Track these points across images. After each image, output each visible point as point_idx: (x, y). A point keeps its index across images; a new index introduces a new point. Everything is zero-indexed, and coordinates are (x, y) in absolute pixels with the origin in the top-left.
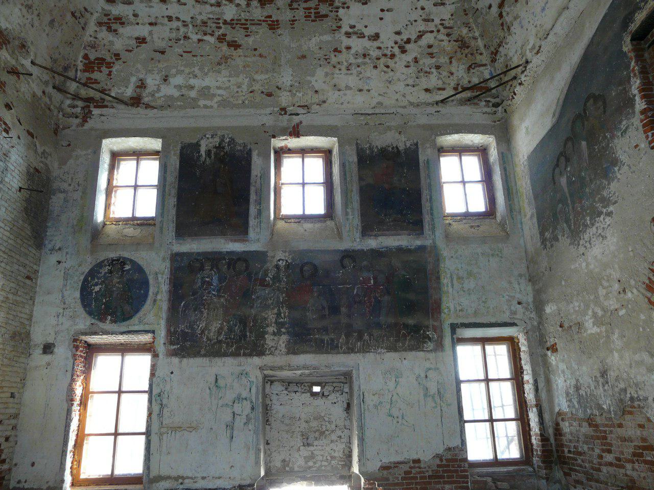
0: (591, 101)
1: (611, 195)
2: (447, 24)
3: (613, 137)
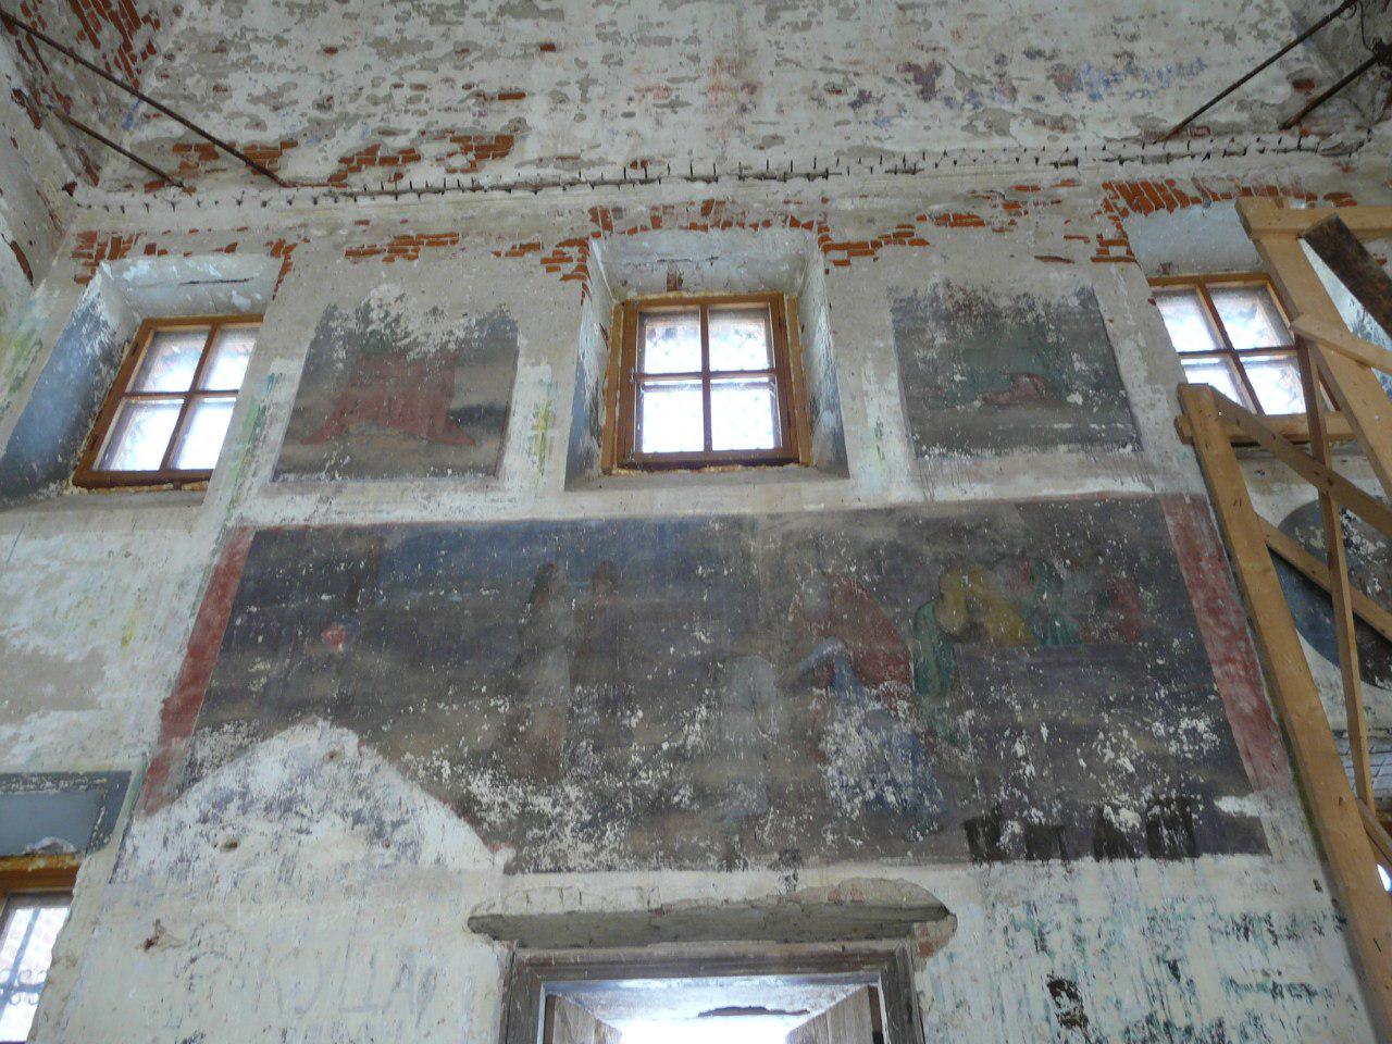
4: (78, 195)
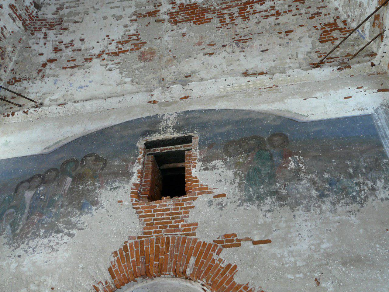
0: (93, 158)
1: (78, 223)
2: (5, 32)
3: (101, 187)
4: (376, 63)
